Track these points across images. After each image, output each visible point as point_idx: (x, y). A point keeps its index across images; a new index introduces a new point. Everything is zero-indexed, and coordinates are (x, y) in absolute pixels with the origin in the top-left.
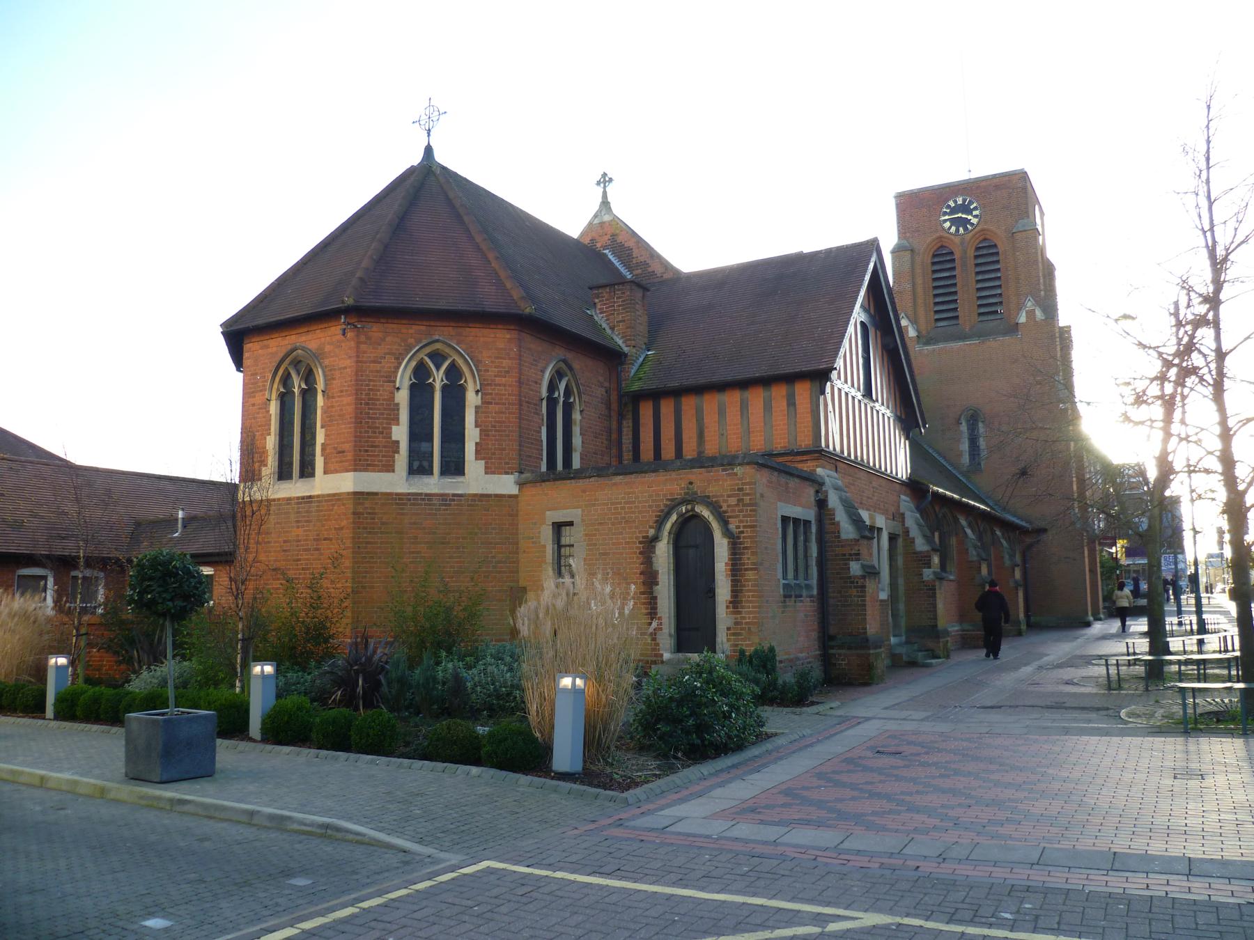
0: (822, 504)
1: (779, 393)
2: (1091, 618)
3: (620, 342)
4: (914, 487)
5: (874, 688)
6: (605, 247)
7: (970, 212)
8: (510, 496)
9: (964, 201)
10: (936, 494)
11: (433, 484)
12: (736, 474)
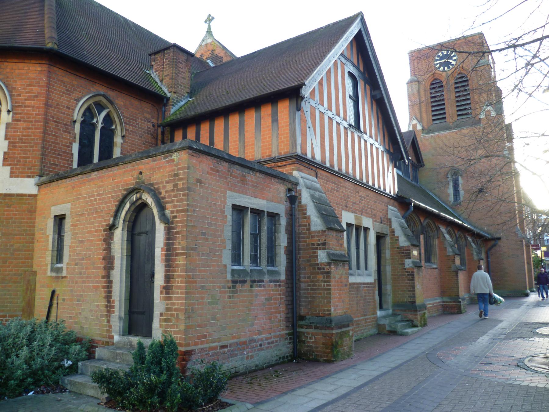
0: (293, 199)
1: (266, 111)
2: (529, 291)
3: (165, 90)
4: (401, 201)
5: (338, 364)
6: (208, 59)
8: (30, 196)
10: (417, 207)
12: (173, 161)
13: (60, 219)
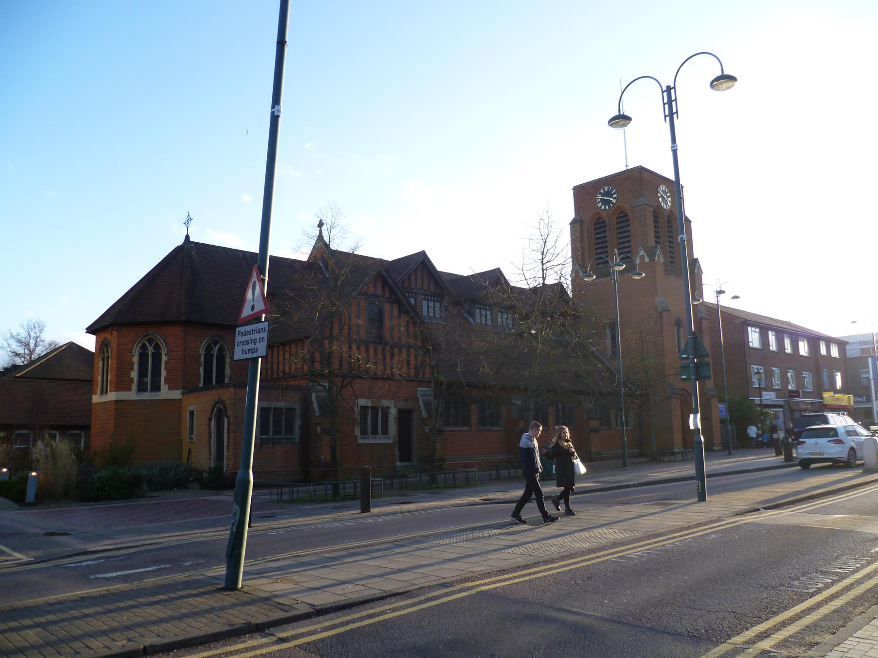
7: (611, 196)
11: (146, 396)
13: (192, 413)
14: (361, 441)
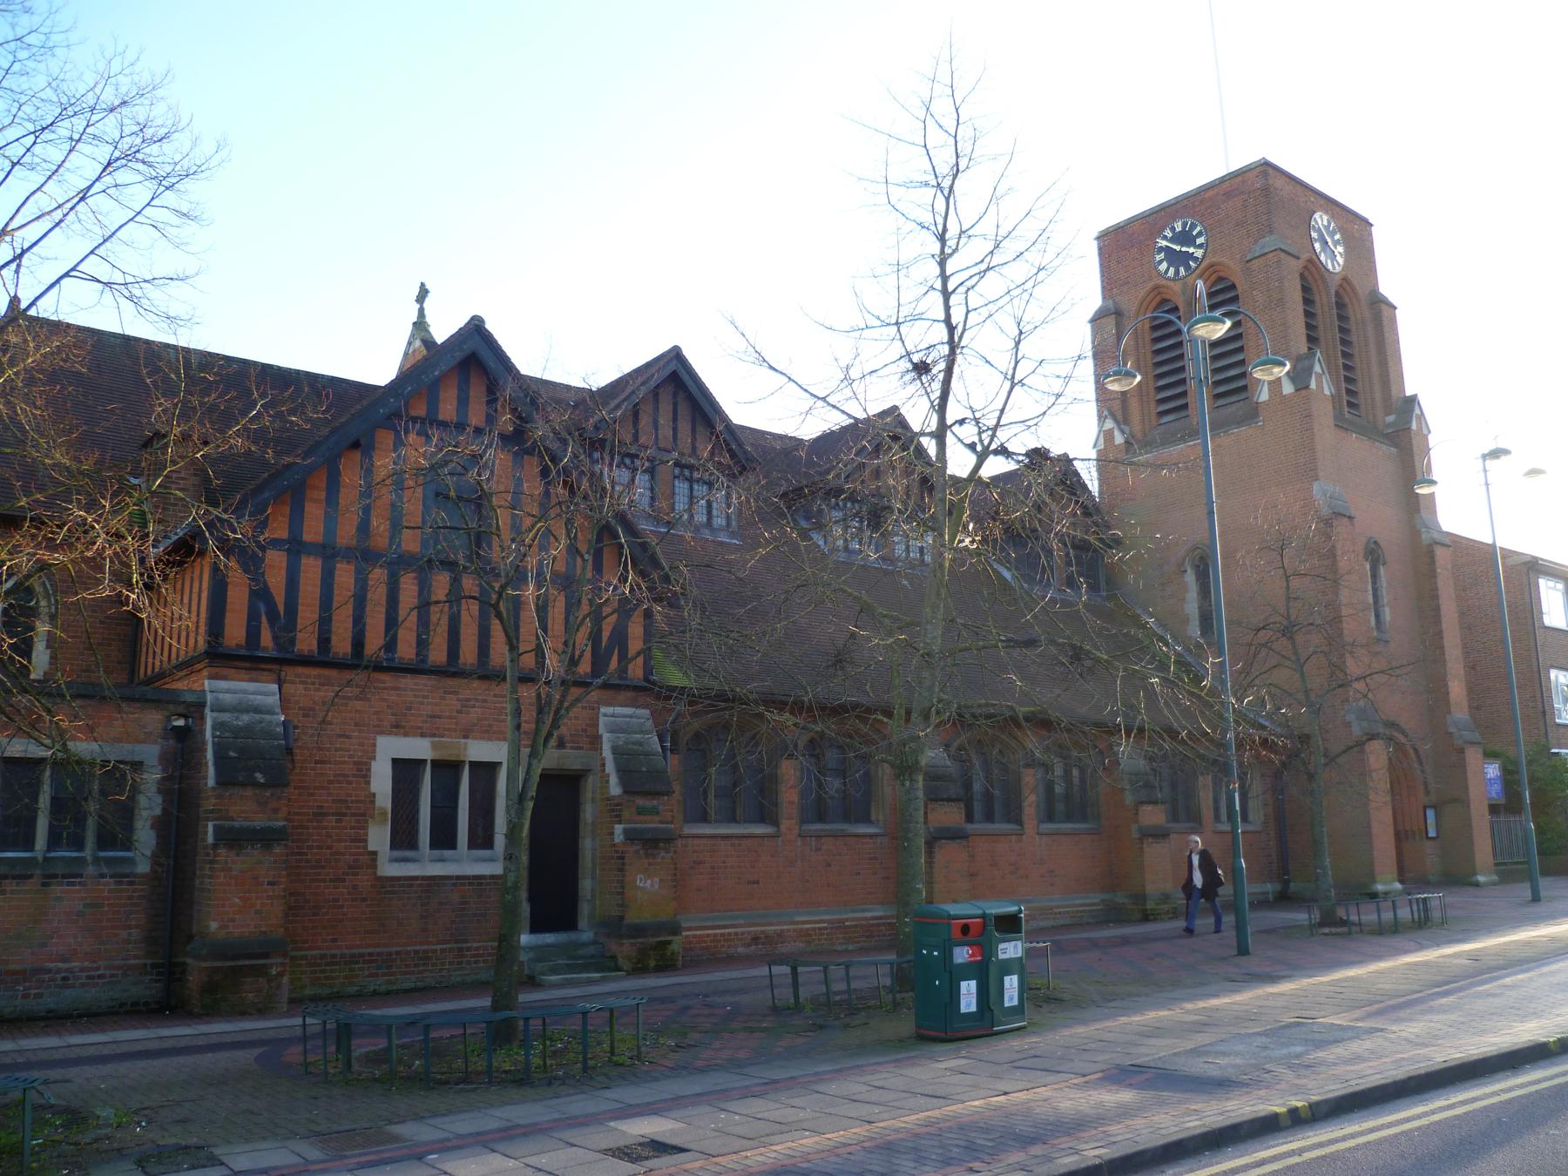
0: (184, 742)
9: (1185, 225)
14: (388, 869)
